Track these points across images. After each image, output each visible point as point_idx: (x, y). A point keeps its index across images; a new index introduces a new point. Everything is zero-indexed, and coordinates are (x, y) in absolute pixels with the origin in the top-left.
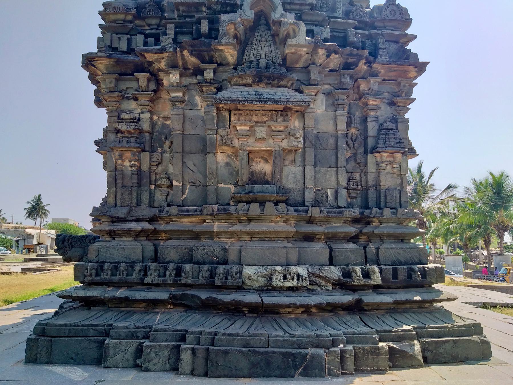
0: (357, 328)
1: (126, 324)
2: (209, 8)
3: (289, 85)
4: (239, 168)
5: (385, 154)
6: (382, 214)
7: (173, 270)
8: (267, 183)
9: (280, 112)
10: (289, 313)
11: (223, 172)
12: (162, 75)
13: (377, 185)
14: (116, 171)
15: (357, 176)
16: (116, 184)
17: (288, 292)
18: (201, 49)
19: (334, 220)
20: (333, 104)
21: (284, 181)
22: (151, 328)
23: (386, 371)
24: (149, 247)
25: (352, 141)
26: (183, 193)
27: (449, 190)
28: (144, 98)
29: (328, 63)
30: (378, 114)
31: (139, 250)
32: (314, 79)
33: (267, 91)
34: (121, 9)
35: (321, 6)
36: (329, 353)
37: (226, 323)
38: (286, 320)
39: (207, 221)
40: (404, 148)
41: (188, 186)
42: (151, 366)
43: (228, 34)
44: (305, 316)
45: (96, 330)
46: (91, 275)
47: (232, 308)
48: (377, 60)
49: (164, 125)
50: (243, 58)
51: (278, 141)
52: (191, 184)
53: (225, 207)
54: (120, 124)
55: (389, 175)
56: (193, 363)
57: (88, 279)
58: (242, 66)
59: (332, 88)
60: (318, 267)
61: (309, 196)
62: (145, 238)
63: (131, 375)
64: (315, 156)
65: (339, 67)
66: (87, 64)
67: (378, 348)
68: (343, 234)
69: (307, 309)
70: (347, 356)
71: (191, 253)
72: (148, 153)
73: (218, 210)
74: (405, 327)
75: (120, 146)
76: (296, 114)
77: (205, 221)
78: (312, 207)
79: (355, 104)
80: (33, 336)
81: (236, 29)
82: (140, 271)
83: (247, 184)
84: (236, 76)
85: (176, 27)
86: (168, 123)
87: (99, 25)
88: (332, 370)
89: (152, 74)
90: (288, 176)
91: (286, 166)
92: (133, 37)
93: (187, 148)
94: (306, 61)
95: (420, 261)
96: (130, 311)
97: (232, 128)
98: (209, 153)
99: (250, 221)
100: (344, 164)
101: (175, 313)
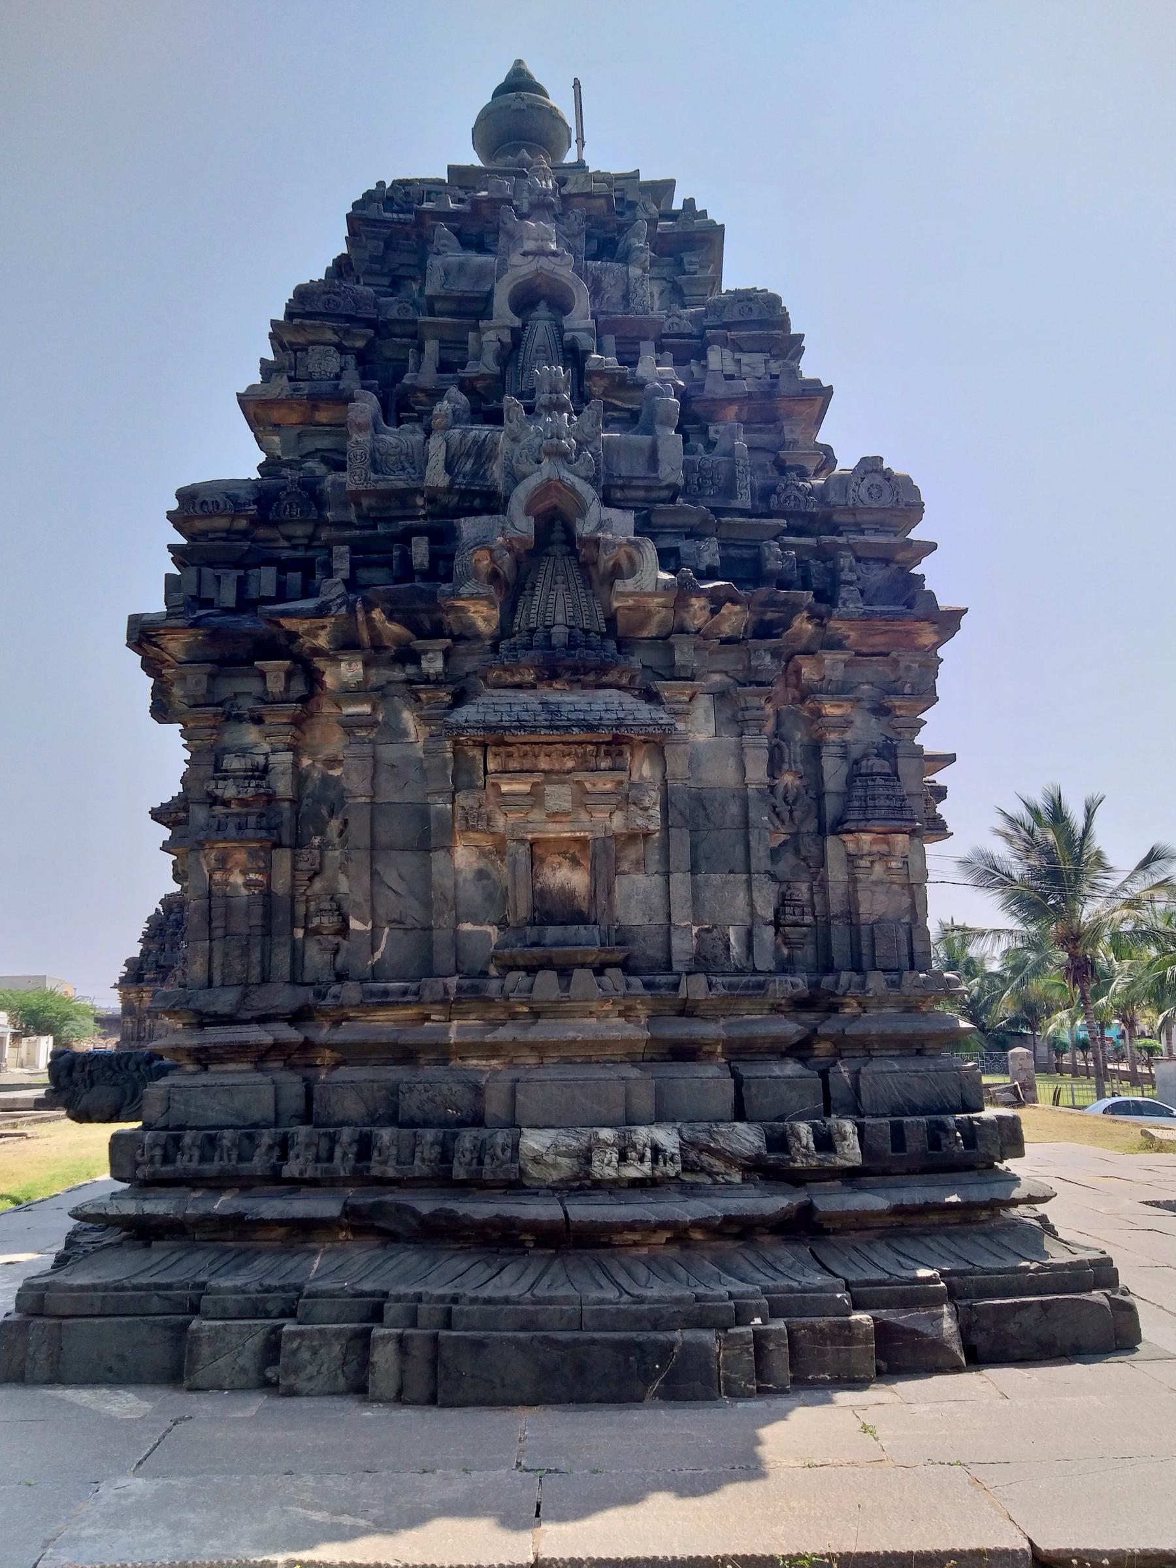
0: (799, 1278)
1: (239, 1282)
2: (431, 500)
3: (624, 681)
4: (507, 882)
5: (866, 837)
6: (862, 985)
7: (350, 1144)
8: (580, 918)
9: (603, 748)
10: (636, 1244)
11: (471, 893)
12: (320, 663)
13: (851, 913)
14: (209, 898)
15: (802, 890)
16: (211, 930)
17: (631, 1192)
18: (414, 606)
19: (745, 1005)
20: (734, 720)
21: (619, 912)
22: (299, 1288)
23: (871, 1381)
24: (292, 1084)
25: (787, 803)
26: (374, 949)
27: (1154, 867)
28: (279, 717)
29: (717, 625)
30: (848, 736)
31: (268, 1096)
32: (683, 666)
33: (571, 700)
34: (222, 506)
35: (699, 485)
36: (726, 1340)
37: (480, 1272)
38: (626, 1261)
39: (433, 1017)
40: (913, 820)
41: (387, 930)
42: (301, 1384)
43: (476, 574)
44: (674, 1251)
45: (167, 1298)
46: (151, 1160)
47: (496, 1235)
48: (835, 611)
49: (326, 780)
50: (512, 622)
51: (600, 815)
52: (393, 925)
53: (477, 981)
54: (221, 784)
55: (879, 889)
56: (402, 1372)
57: (144, 1171)
58: (513, 640)
59: (732, 681)
60: (706, 1125)
61: (683, 946)
62: (281, 1064)
63: (256, 1404)
64: (694, 847)
65: (745, 632)
66: (140, 640)
67: (849, 1326)
68: (769, 1040)
69: (679, 1234)
70: (772, 1346)
71: (394, 1099)
72: (287, 852)
73: (459, 989)
74: (923, 1273)
75: (220, 838)
76: (645, 747)
77: (427, 1018)
78: (688, 974)
79: (791, 712)
80: (14, 1317)
81: (493, 561)
82: (270, 1147)
83: (528, 924)
84: (496, 669)
85: (354, 550)
86: (336, 772)
87: (169, 547)
88: (735, 1381)
89: (297, 658)
90: (629, 897)
91: (623, 873)
92: (251, 572)
93: (383, 837)
94: (662, 623)
95: (963, 1101)
96: (248, 1250)
97: (489, 790)
98: (436, 849)
99: (536, 1015)
100: (766, 864)
101: (357, 1251)
